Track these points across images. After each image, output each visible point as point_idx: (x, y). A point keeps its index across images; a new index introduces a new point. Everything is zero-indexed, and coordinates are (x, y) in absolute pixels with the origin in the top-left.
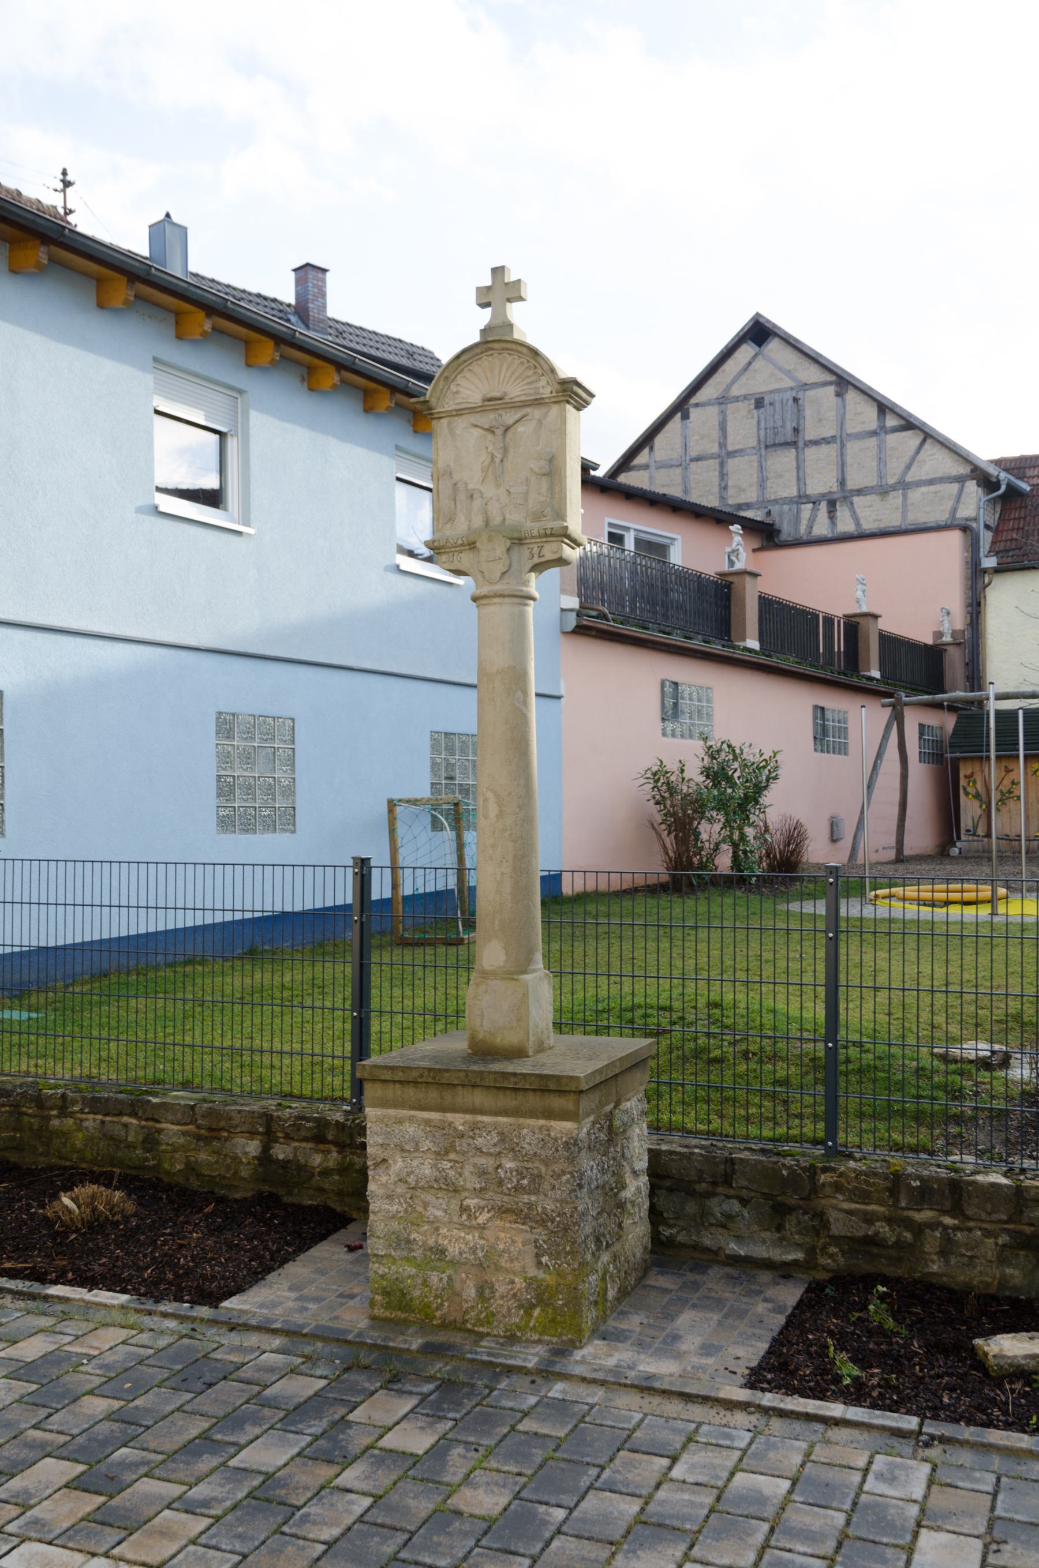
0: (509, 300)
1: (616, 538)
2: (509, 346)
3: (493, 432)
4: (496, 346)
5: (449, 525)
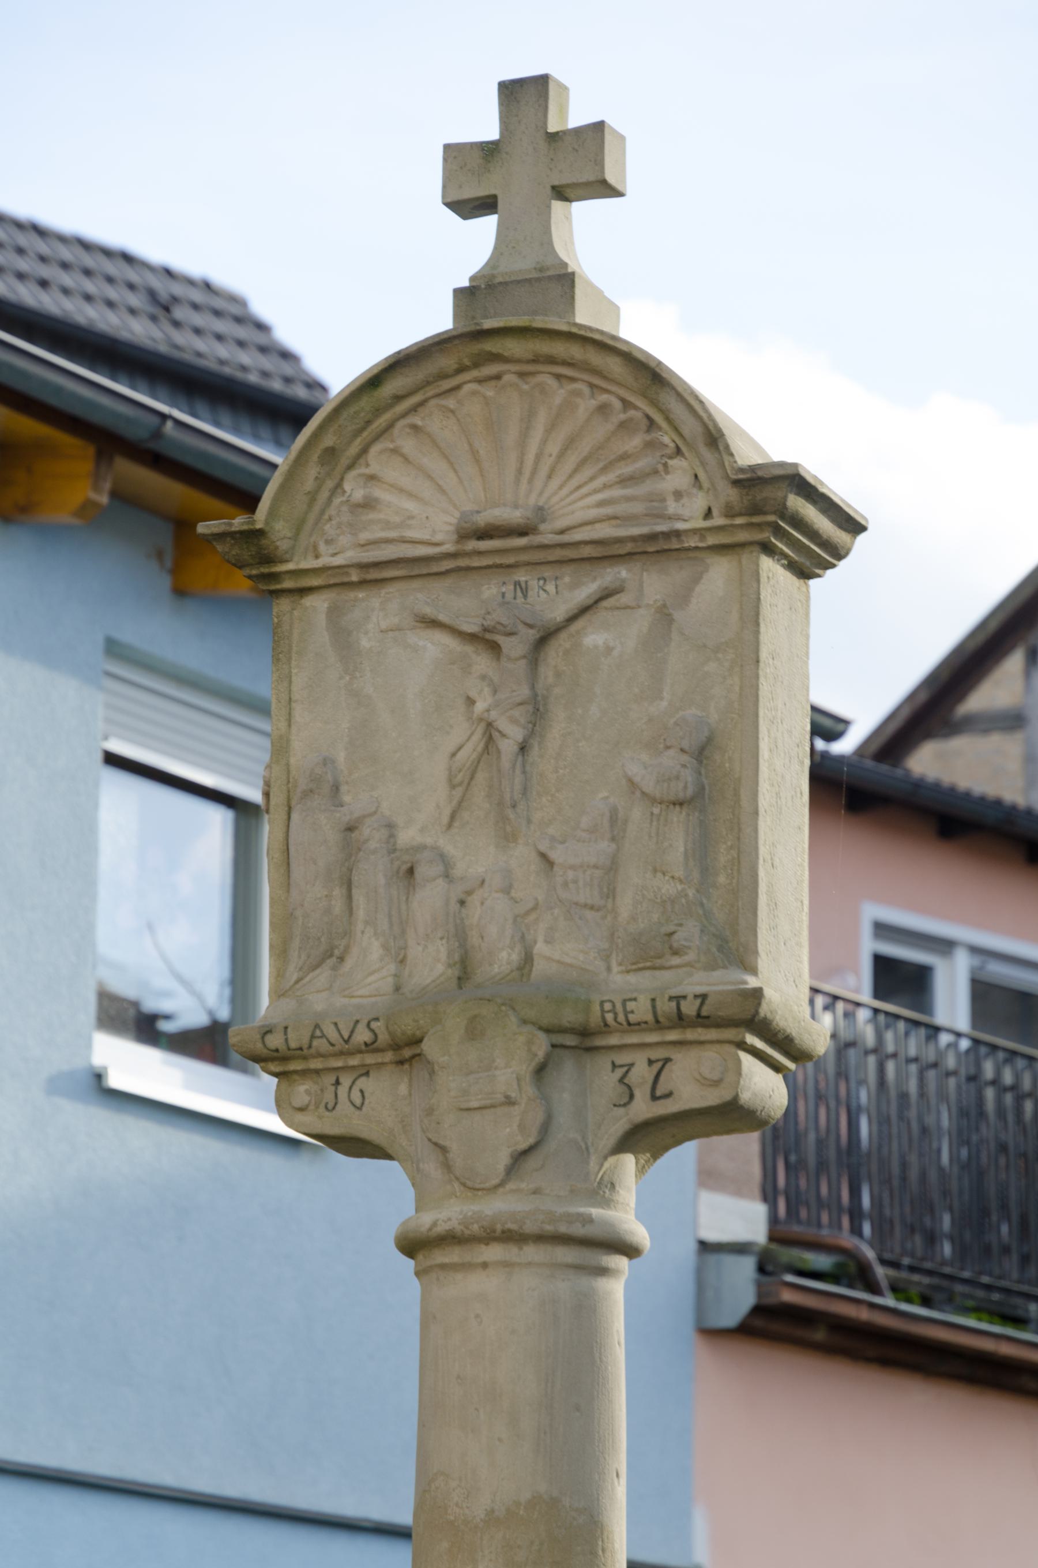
0: (563, 193)
1: (900, 981)
2: (559, 349)
3: (494, 648)
4: (512, 347)
5: (323, 976)
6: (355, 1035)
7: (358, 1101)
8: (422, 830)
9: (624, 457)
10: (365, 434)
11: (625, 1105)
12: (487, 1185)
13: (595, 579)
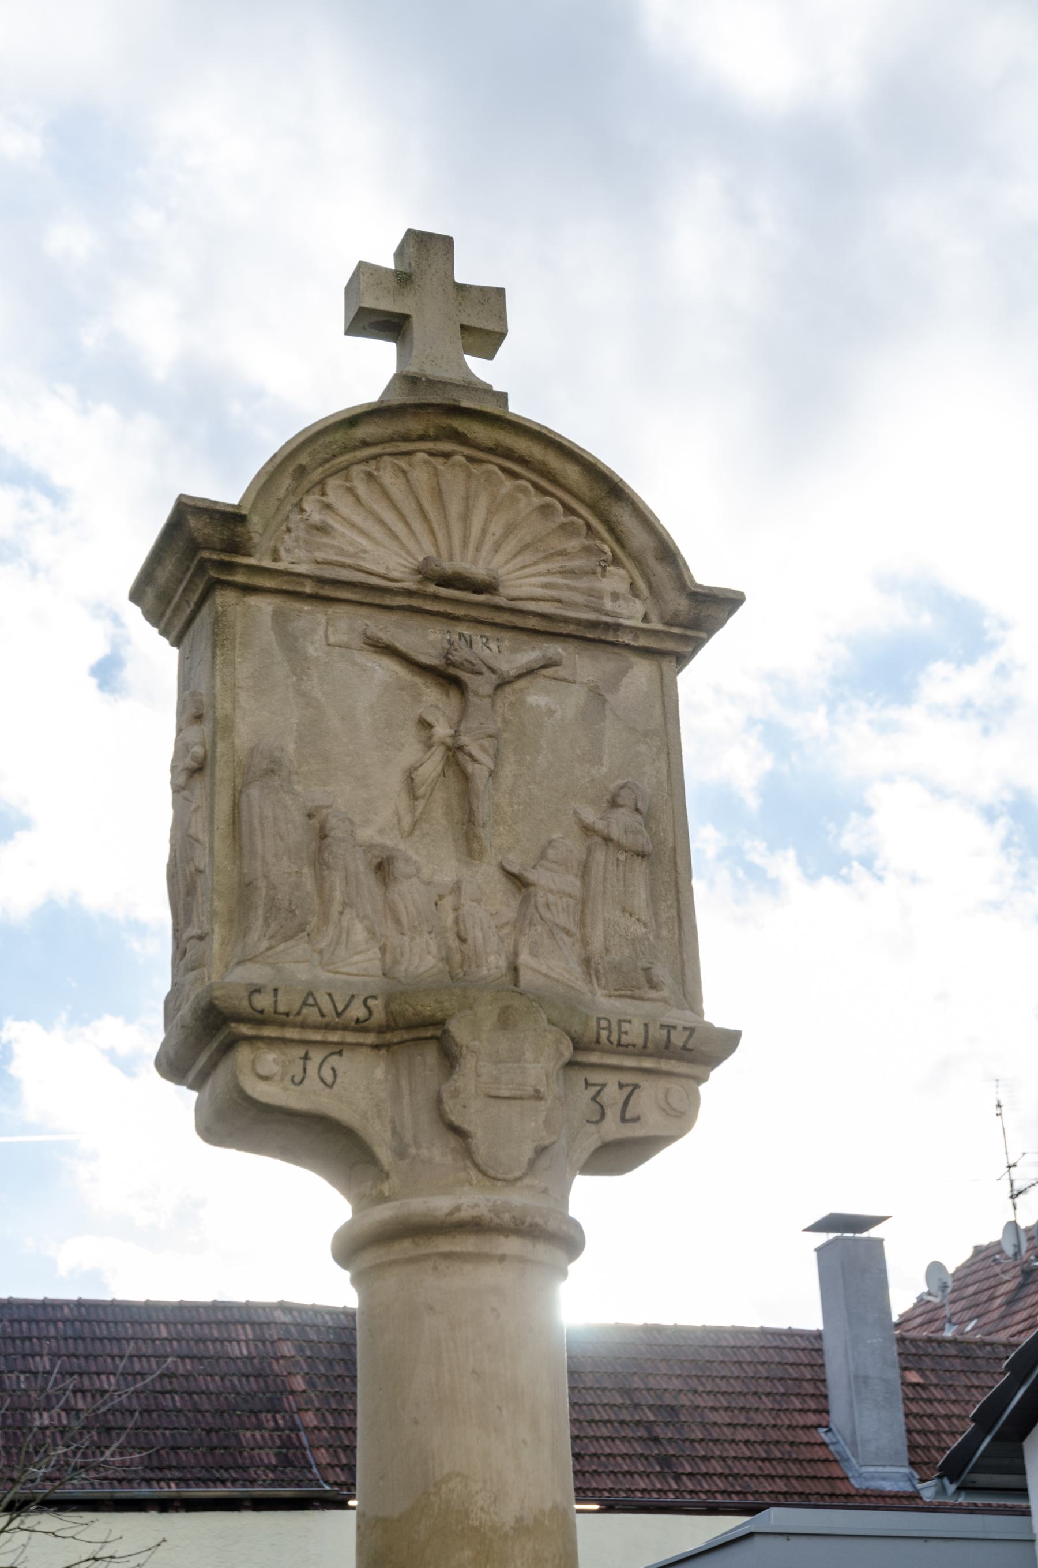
6: (349, 1009)
7: (329, 1079)
8: (381, 832)
9: (563, 553)
10: (327, 466)
11: (597, 1122)
12: (509, 1176)
13: (534, 649)
